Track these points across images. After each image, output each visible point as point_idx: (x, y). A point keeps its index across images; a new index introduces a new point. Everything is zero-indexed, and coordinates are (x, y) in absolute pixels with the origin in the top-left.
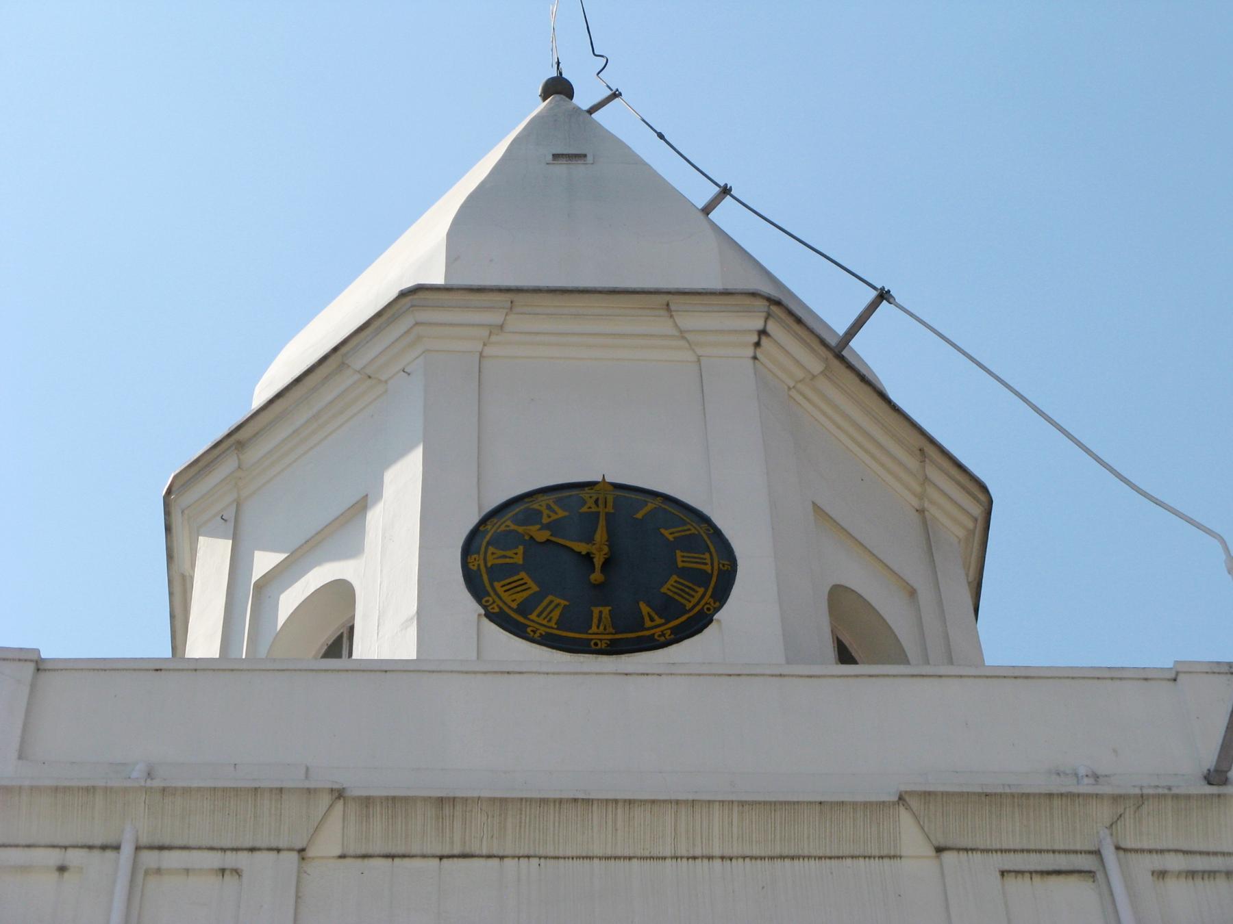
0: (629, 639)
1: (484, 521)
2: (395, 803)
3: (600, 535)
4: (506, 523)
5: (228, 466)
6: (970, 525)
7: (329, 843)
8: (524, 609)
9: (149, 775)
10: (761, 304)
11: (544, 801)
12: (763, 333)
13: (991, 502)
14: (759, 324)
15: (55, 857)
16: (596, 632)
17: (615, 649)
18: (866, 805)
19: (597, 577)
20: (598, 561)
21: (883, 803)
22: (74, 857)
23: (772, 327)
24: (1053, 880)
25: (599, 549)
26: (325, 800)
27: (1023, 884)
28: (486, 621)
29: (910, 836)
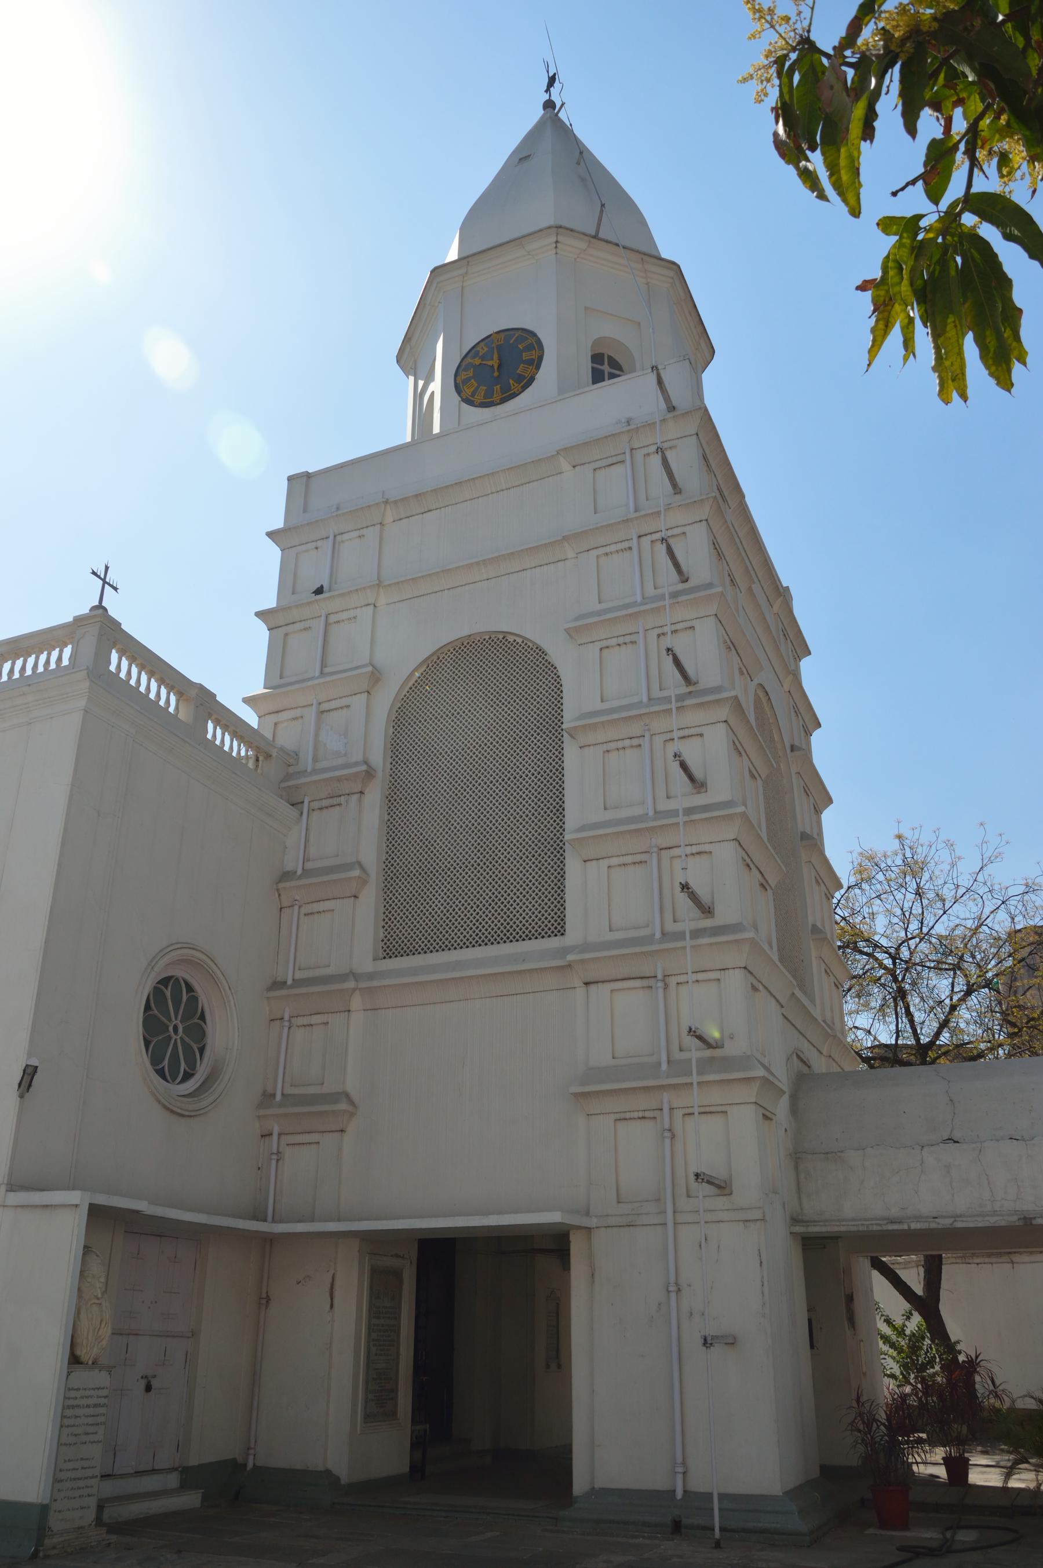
0: (508, 396)
1: (462, 361)
2: (404, 500)
3: (496, 356)
4: (469, 360)
5: (408, 350)
6: (671, 280)
7: (389, 518)
8: (473, 395)
9: (338, 509)
10: (554, 230)
11: (447, 487)
12: (557, 242)
13: (679, 267)
14: (555, 239)
15: (314, 545)
16: (496, 397)
17: (503, 401)
18: (548, 458)
19: (496, 374)
20: (496, 367)
21: (553, 456)
22: (319, 543)
23: (560, 238)
24: (612, 467)
25: (494, 362)
26: (383, 506)
27: (602, 472)
28: (464, 405)
29: (564, 464)
